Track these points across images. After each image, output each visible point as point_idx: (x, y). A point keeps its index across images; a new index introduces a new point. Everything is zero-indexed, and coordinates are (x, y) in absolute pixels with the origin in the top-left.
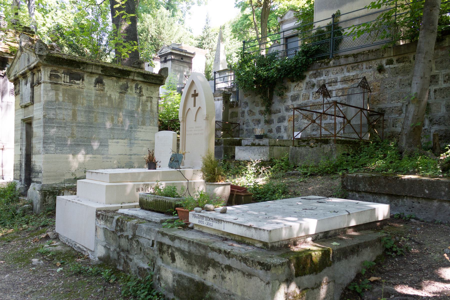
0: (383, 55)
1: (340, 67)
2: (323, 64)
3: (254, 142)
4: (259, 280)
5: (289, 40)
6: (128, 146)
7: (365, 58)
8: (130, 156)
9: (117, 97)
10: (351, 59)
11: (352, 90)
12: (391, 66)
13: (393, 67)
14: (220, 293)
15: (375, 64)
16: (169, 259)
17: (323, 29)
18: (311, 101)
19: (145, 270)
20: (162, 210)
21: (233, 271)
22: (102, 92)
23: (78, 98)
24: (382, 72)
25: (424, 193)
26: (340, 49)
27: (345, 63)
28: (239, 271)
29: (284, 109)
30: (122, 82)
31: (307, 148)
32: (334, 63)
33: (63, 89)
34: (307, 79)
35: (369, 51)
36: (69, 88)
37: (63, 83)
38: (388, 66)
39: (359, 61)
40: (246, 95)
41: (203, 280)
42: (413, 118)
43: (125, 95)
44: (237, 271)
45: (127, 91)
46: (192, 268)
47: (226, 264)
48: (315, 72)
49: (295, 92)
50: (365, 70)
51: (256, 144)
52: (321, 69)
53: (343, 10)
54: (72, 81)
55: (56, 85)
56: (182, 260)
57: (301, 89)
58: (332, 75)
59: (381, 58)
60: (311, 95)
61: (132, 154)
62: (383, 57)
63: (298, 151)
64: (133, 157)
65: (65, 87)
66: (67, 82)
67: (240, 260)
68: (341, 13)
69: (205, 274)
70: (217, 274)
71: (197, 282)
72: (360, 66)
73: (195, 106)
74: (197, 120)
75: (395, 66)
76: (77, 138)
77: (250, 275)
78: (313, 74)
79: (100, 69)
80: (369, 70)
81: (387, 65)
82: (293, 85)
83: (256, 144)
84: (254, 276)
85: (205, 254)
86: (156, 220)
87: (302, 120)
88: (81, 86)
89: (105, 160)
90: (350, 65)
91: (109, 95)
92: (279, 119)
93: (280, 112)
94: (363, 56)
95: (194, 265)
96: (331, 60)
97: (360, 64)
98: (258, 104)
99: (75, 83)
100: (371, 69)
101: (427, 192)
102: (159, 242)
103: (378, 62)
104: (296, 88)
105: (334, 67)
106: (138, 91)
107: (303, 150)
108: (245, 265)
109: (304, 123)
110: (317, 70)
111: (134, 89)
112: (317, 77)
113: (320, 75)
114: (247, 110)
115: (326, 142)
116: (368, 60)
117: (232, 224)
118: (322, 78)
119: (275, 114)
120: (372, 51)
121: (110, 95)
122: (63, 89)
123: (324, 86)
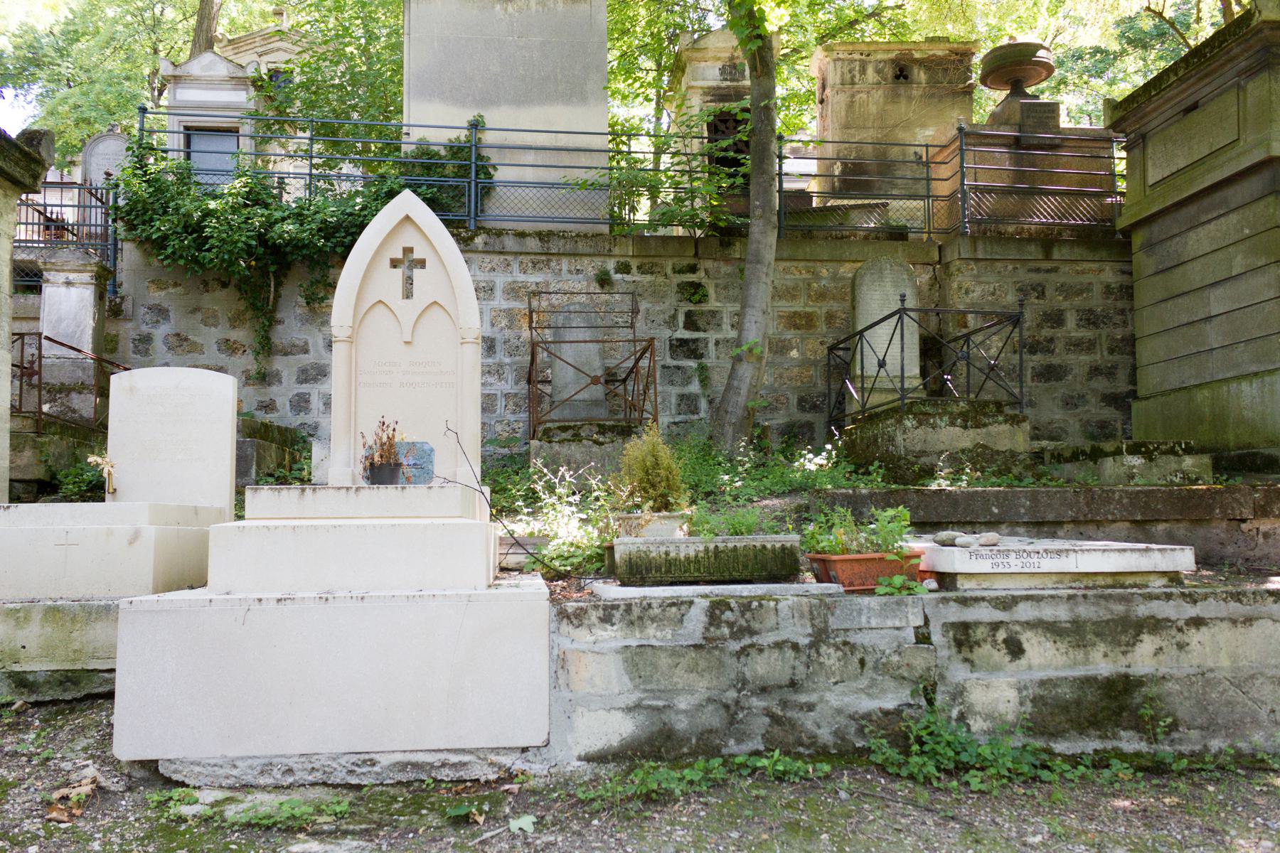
1: (502, 257)
4: (1270, 623)
5: (198, 143)
7: (569, 247)
10: (533, 244)
11: (566, 318)
12: (628, 278)
14: (1177, 679)
15: (590, 266)
16: (1001, 656)
17: (435, 148)
19: (897, 712)
20: (746, 574)
21: (1206, 624)
25: (992, 514)
26: (489, 212)
27: (516, 248)
28: (1222, 620)
31: (584, 446)
38: (619, 276)
40: (159, 284)
41: (1123, 670)
42: (749, 391)
44: (1218, 622)
46: (1086, 654)
47: (1187, 617)
50: (565, 275)
53: (493, 117)
56: (1049, 645)
62: (609, 254)
67: (1224, 600)
69: (1129, 655)
70: (1164, 644)
71: (1107, 679)
72: (553, 264)
73: (408, 294)
77: (1249, 621)
80: (574, 277)
84: (1257, 619)
85: (1128, 611)
90: (530, 257)
93: (306, 351)
95: (1094, 645)
97: (554, 258)
98: (215, 317)
100: (581, 276)
101: (996, 511)
102: (953, 625)
103: (598, 261)
105: (484, 252)
108: (1238, 604)
114: (160, 332)
116: (575, 255)
117: (1099, 554)
119: (286, 354)
120: (586, 236)
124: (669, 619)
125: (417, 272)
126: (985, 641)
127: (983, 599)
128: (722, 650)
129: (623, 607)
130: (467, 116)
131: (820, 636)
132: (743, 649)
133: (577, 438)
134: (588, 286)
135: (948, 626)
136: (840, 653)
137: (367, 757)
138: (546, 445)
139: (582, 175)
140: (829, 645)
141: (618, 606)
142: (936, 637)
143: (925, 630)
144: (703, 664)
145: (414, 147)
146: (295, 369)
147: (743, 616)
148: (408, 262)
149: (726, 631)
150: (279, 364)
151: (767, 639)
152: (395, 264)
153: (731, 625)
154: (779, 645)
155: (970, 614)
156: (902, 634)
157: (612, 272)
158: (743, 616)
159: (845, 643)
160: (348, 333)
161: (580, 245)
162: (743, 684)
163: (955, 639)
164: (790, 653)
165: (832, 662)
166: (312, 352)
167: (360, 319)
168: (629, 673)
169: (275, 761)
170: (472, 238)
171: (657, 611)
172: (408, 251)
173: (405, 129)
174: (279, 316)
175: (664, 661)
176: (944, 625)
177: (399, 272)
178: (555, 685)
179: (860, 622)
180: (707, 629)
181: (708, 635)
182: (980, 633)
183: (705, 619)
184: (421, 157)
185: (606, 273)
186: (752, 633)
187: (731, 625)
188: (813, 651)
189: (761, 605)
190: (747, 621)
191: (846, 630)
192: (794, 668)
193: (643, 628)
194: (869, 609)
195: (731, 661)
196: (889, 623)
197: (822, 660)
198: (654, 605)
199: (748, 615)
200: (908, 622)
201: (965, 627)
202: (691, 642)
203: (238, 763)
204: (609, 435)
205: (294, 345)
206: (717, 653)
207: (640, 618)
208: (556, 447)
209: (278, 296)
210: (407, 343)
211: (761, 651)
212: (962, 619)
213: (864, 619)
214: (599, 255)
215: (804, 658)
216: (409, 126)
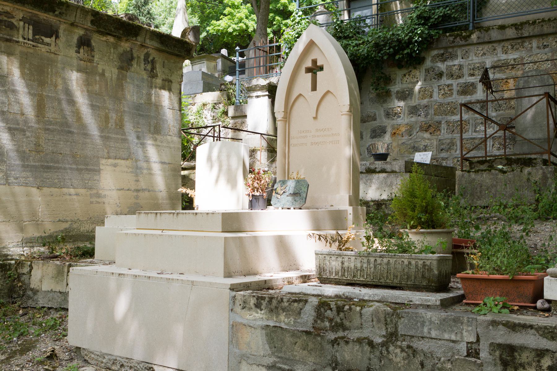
1: (490, 45)
2: (458, 39)
3: (372, 167)
6: (132, 172)
8: (135, 194)
9: (115, 76)
10: (511, 33)
18: (436, 101)
22: (89, 64)
23: (48, 74)
27: (500, 37)
29: (382, 113)
30: (125, 45)
32: (478, 38)
33: (21, 52)
34: (428, 63)
36: (31, 51)
37: (21, 39)
39: (525, 35)
43: (128, 74)
45: (132, 65)
48: (442, 52)
49: (405, 86)
50: (535, 51)
51: (377, 170)
52: (453, 47)
54: (37, 37)
55: (8, 44)
57: (416, 80)
58: (474, 58)
60: (436, 90)
61: (139, 188)
63: (474, 179)
64: (141, 194)
65: (25, 50)
66: (29, 40)
73: (314, 88)
74: (319, 117)
76: (47, 154)
78: (438, 56)
79: (90, 18)
82: (400, 73)
83: (377, 170)
86: (429, 301)
87: (419, 133)
88: (53, 48)
89: (94, 200)
90: (509, 43)
91: (101, 71)
94: (532, 27)
96: (472, 33)
97: (526, 40)
99: (43, 43)
100: (547, 50)
102: (500, 345)
104: (405, 79)
106: (149, 67)
107: (485, 178)
109: (424, 139)
110: (446, 48)
111: (143, 62)
112: (445, 60)
113: (453, 57)
115: (528, 162)
118: (456, 62)
121: (103, 71)
122: (21, 52)
123: (486, 72)
124: (293, 311)
125: (319, 74)
126: (530, 364)
127: (531, 327)
128: (322, 337)
129: (267, 299)
131: (392, 337)
132: (336, 339)
135: (495, 347)
136: (404, 354)
137: (150, 366)
140: (396, 347)
141: (265, 298)
142: (484, 354)
143: (474, 346)
144: (311, 345)
146: (370, 130)
147: (338, 314)
148: (315, 69)
149: (327, 324)
151: (354, 335)
153: (331, 320)
154: (359, 341)
155: (517, 339)
156: (458, 347)
158: (338, 314)
159: (409, 347)
162: (336, 365)
163: (501, 359)
164: (367, 348)
165: (398, 359)
166: (378, 119)
168: (269, 343)
169: (118, 358)
170: (469, 36)
171: (286, 304)
172: (314, 62)
175: (288, 339)
176: (491, 344)
178: (230, 342)
179: (422, 332)
180: (315, 321)
181: (316, 325)
182: (524, 357)
183: (314, 314)
186: (345, 329)
187: (331, 320)
188: (384, 348)
189: (350, 309)
190: (341, 320)
191: (412, 337)
192: (370, 359)
193: (278, 314)
194: (431, 322)
195: (329, 347)
196: (446, 336)
197: (391, 357)
198: (285, 300)
199: (342, 315)
200: (462, 337)
201: (511, 349)
202: (305, 329)
203: (106, 357)
204: (514, 166)
206: (319, 339)
207: (276, 308)
211: (347, 342)
212: (508, 342)
213: (426, 330)
215: (377, 353)
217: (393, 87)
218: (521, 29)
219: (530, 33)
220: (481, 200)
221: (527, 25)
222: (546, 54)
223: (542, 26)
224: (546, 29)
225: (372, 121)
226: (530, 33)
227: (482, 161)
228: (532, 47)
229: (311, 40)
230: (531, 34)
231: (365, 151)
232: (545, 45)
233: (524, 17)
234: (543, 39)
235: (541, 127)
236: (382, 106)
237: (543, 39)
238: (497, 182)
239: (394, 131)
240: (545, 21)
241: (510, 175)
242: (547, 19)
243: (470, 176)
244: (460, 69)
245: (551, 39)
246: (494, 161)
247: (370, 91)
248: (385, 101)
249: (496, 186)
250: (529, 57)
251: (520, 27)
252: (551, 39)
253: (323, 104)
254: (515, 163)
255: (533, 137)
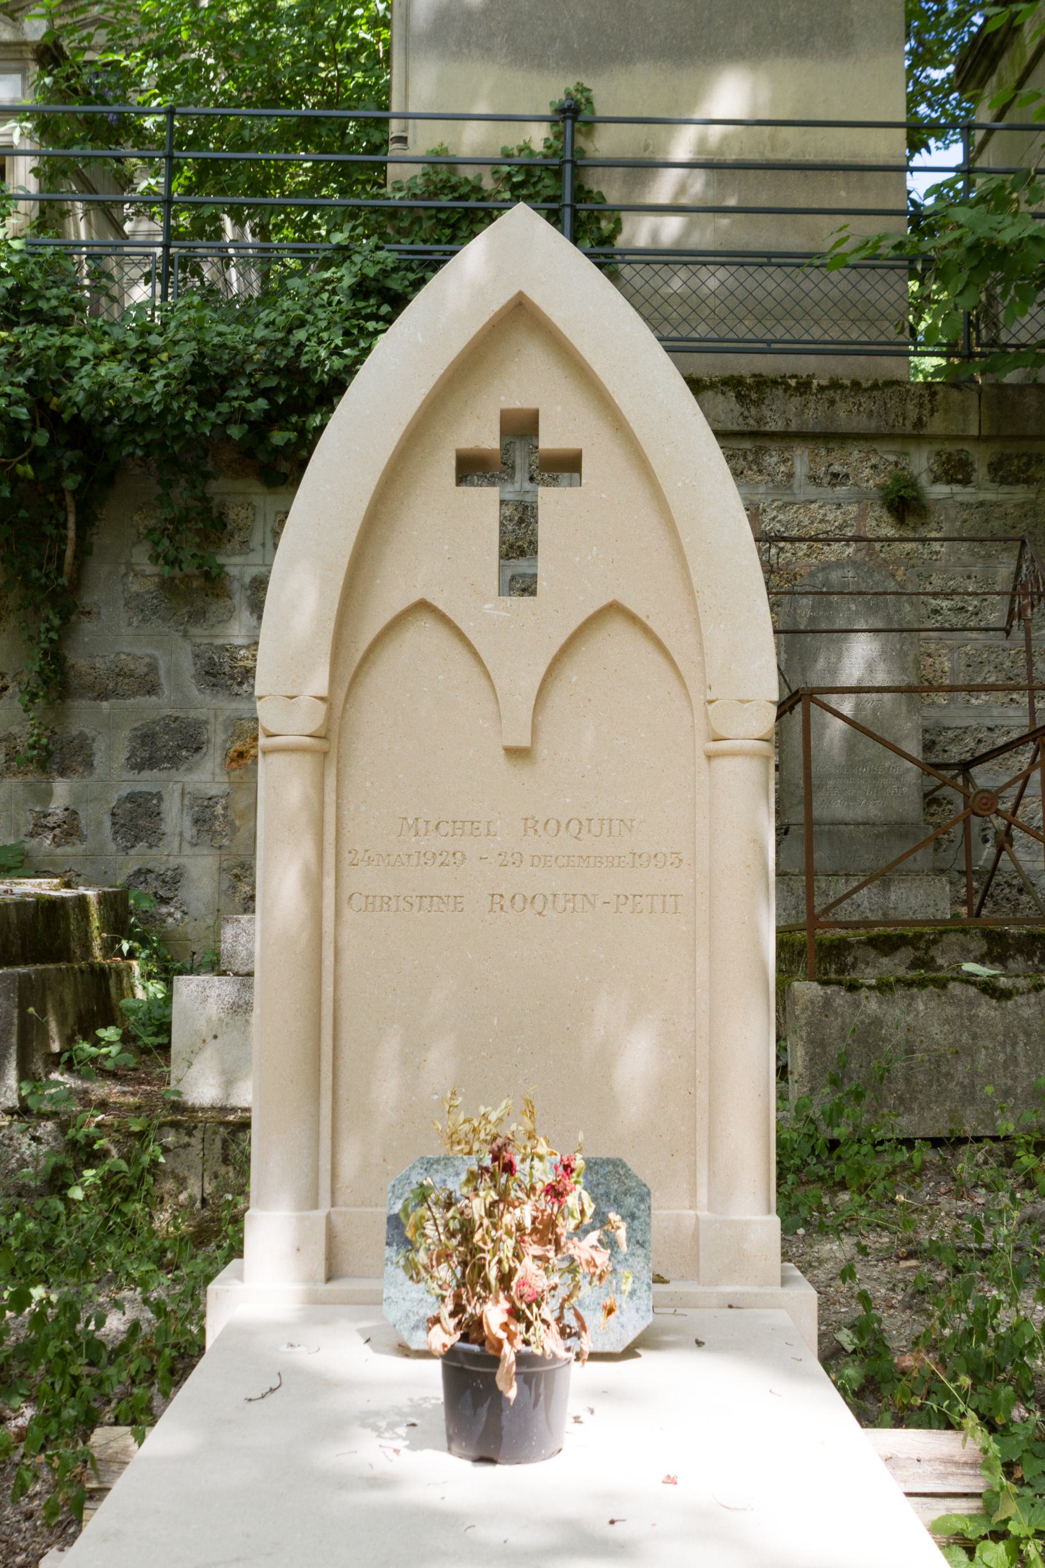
0: (919, 423)
13: (972, 499)
15: (867, 470)
17: (468, 173)
24: (911, 520)
29: (188, 666)
31: (954, 1001)
35: (835, 385)
38: (940, 490)
39: (771, 427)
50: (803, 490)
53: (613, 92)
59: (905, 437)
63: (877, 1022)
68: (902, 133)
75: (982, 496)
80: (826, 492)
81: (936, 480)
92: (146, 738)
94: (796, 400)
97: (772, 446)
100: (841, 491)
103: (887, 454)
125: (552, 502)
130: (549, 90)
133: (927, 975)
134: (862, 516)
138: (841, 998)
139: (822, 234)
145: (417, 170)
146: (126, 733)
148: (520, 462)
150: (85, 717)
152: (471, 468)
157: (924, 480)
160: (314, 724)
161: (842, 411)
167: (354, 655)
172: (521, 427)
173: (395, 128)
174: (88, 599)
177: (485, 503)
184: (433, 195)
185: (912, 484)
204: (1017, 964)
205: (121, 673)
208: (872, 1005)
209: (83, 551)
210: (516, 754)
214: (891, 437)
216: (405, 117)
217: (238, 560)
218: (758, 403)
219: (788, 421)
220: (910, 1110)
221: (780, 392)
222: (839, 506)
223: (832, 402)
224: (846, 416)
225: (134, 694)
226: (788, 421)
227: (888, 938)
228: (790, 475)
229: (521, 294)
230: (794, 427)
231: (100, 823)
232: (835, 475)
233: (744, 359)
234: (829, 451)
235: (875, 777)
236: (185, 635)
237: (829, 451)
238: (975, 1037)
239: (238, 746)
240: (842, 387)
241: (1026, 1007)
242: (847, 382)
243: (857, 1005)
244: (521, 521)
245: (856, 454)
246: (935, 942)
247: (129, 565)
248: (198, 616)
249: (970, 1052)
250: (779, 509)
251: (754, 396)
252: (856, 454)
253: (573, 674)
254: (1020, 951)
255: (850, 815)
